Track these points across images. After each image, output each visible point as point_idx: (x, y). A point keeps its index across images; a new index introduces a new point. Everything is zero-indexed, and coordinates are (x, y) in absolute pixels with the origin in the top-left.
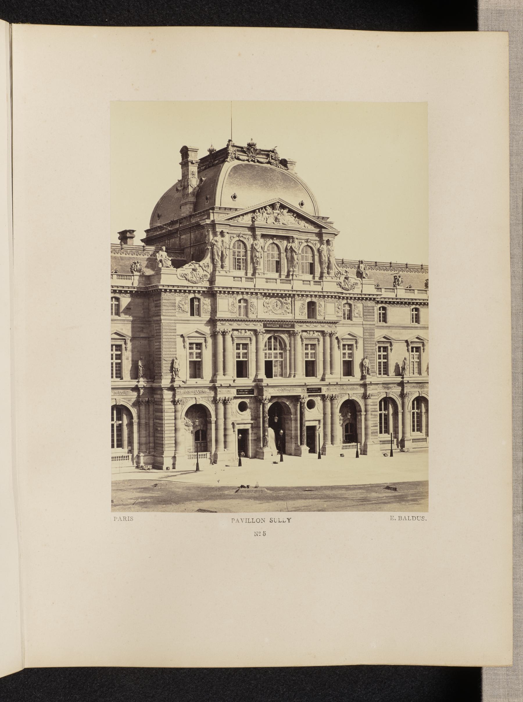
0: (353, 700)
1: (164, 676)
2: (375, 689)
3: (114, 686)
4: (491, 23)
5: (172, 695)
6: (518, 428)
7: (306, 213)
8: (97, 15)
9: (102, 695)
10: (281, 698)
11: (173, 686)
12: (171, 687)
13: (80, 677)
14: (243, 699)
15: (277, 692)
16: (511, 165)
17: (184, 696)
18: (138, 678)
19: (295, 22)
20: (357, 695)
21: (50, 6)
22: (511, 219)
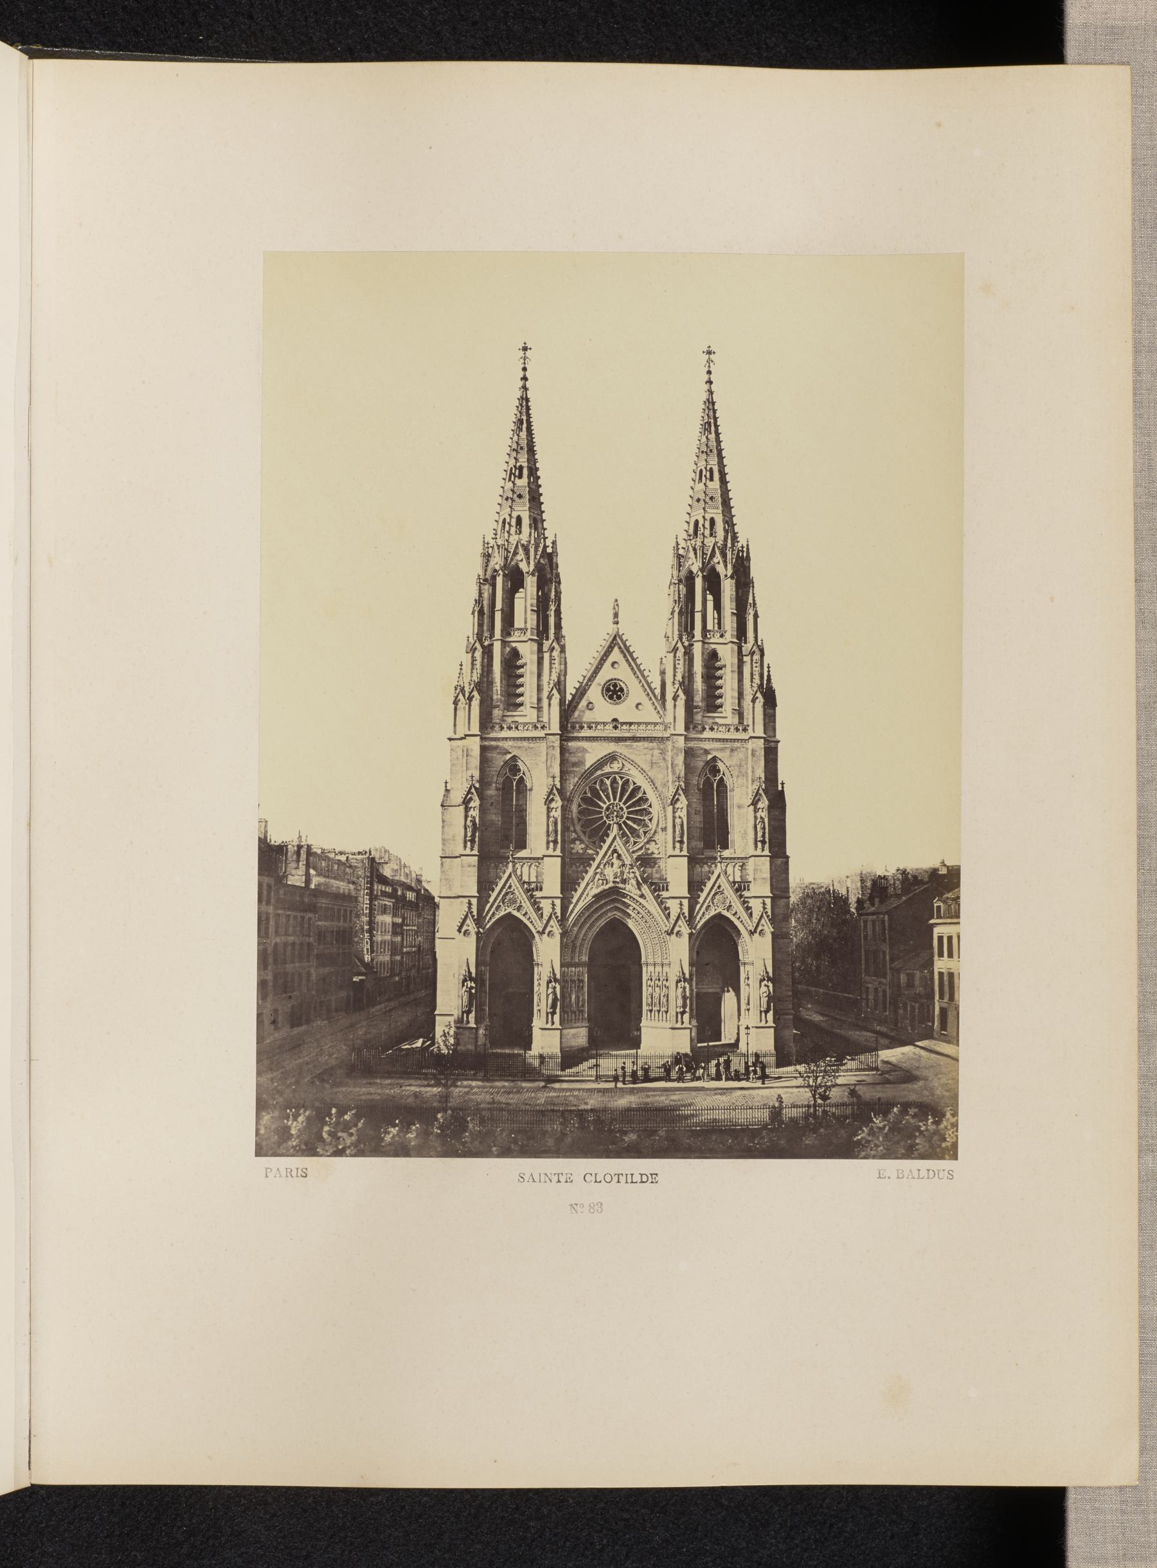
0: (759, 1564)
1: (332, 1511)
2: (809, 1538)
3: (221, 1532)
4: (1095, 55)
5: (350, 1552)
6: (1148, 961)
7: (28, 135)
8: (180, 26)
9: (192, 1552)
10: (595, 1561)
11: (353, 1532)
12: (349, 1534)
13: (145, 1513)
14: (511, 1562)
15: (588, 1545)
16: (1137, 372)
17: (378, 1555)
18: (274, 1515)
19: (626, 42)
20: (768, 1553)
21: (75, 10)
22: (1136, 495)
